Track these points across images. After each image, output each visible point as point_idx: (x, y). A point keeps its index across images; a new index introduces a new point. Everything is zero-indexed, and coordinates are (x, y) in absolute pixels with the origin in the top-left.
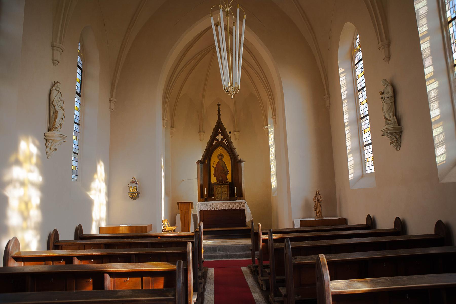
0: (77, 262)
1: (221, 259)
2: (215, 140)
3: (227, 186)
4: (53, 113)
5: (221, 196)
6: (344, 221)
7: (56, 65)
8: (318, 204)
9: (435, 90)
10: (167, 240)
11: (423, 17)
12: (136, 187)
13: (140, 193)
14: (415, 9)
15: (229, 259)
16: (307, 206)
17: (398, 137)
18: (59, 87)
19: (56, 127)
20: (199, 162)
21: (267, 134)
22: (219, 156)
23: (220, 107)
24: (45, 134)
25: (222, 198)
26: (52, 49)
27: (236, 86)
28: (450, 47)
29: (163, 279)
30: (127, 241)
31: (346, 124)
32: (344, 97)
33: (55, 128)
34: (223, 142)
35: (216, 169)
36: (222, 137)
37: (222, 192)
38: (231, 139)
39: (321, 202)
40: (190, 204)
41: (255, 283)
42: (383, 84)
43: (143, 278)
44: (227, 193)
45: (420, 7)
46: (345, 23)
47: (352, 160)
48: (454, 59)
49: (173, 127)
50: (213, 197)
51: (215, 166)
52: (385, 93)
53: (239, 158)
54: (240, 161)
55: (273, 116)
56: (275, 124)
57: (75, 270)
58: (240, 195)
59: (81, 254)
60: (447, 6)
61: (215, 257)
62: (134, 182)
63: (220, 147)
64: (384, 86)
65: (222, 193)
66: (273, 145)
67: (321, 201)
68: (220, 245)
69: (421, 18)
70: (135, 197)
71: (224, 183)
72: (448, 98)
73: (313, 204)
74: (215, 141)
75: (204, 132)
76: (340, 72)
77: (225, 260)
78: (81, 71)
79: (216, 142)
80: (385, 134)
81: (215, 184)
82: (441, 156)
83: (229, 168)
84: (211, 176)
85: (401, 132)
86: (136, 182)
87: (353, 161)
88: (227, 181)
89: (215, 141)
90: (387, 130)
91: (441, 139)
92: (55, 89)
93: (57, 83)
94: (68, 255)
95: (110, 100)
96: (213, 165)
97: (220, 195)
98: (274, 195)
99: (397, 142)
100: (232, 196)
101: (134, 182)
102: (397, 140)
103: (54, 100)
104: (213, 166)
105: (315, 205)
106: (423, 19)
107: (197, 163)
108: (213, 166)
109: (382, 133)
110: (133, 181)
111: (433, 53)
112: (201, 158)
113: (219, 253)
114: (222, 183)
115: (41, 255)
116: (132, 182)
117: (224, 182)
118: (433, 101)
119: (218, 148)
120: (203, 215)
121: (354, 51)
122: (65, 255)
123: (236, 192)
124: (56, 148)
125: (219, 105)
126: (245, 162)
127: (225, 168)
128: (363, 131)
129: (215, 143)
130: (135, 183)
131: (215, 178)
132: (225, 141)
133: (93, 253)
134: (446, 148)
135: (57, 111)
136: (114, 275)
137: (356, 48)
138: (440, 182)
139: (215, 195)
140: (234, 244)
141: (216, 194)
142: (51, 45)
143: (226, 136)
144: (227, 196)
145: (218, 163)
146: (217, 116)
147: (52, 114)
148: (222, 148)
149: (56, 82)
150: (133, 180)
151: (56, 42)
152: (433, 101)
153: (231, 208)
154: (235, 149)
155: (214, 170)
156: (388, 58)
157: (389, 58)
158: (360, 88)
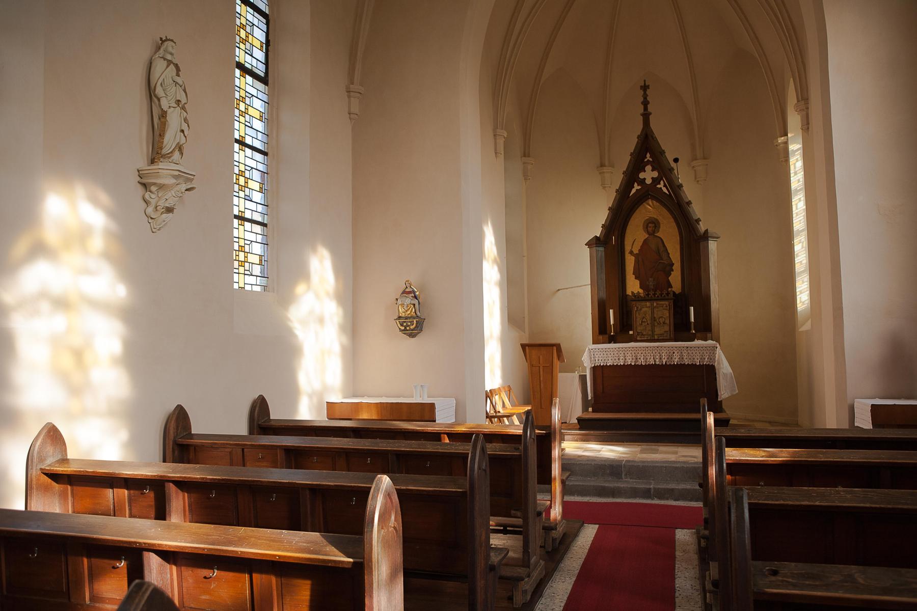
1: (629, 498)
2: (658, 186)
3: (667, 303)
4: (158, 117)
5: (650, 328)
10: (437, 449)
12: (414, 305)
13: (425, 319)
15: (653, 499)
18: (170, 49)
19: (168, 154)
20: (594, 243)
23: (647, 92)
24: (140, 172)
25: (653, 335)
33: (164, 156)
34: (658, 186)
36: (655, 174)
37: (653, 319)
38: (679, 178)
40: (555, 348)
41: (697, 590)
44: (667, 321)
49: (529, 156)
50: (631, 332)
51: (636, 251)
53: (702, 227)
54: (706, 236)
55: (798, 101)
56: (806, 126)
58: (705, 328)
59: (180, 477)
61: (613, 493)
62: (410, 293)
63: (650, 200)
65: (655, 320)
66: (800, 190)
68: (635, 462)
70: (412, 330)
71: (658, 296)
74: (636, 184)
77: (643, 504)
78: (264, 21)
79: (639, 187)
81: (637, 298)
83: (675, 254)
86: (414, 292)
88: (670, 289)
89: (636, 184)
92: (161, 56)
93: (167, 40)
94: (151, 475)
96: (632, 248)
97: (649, 328)
101: (410, 293)
104: (631, 253)
107: (589, 244)
110: (407, 290)
112: (598, 232)
113: (625, 483)
116: (404, 292)
117: (658, 293)
120: (603, 377)
123: (692, 320)
124: (168, 205)
125: (645, 88)
129: (637, 190)
131: (637, 282)
139: (636, 327)
140: (672, 458)
141: (638, 324)
143: (665, 171)
144: (667, 328)
145: (645, 242)
148: (655, 202)
149: (164, 38)
150: (407, 287)
153: (676, 360)
154: (689, 203)
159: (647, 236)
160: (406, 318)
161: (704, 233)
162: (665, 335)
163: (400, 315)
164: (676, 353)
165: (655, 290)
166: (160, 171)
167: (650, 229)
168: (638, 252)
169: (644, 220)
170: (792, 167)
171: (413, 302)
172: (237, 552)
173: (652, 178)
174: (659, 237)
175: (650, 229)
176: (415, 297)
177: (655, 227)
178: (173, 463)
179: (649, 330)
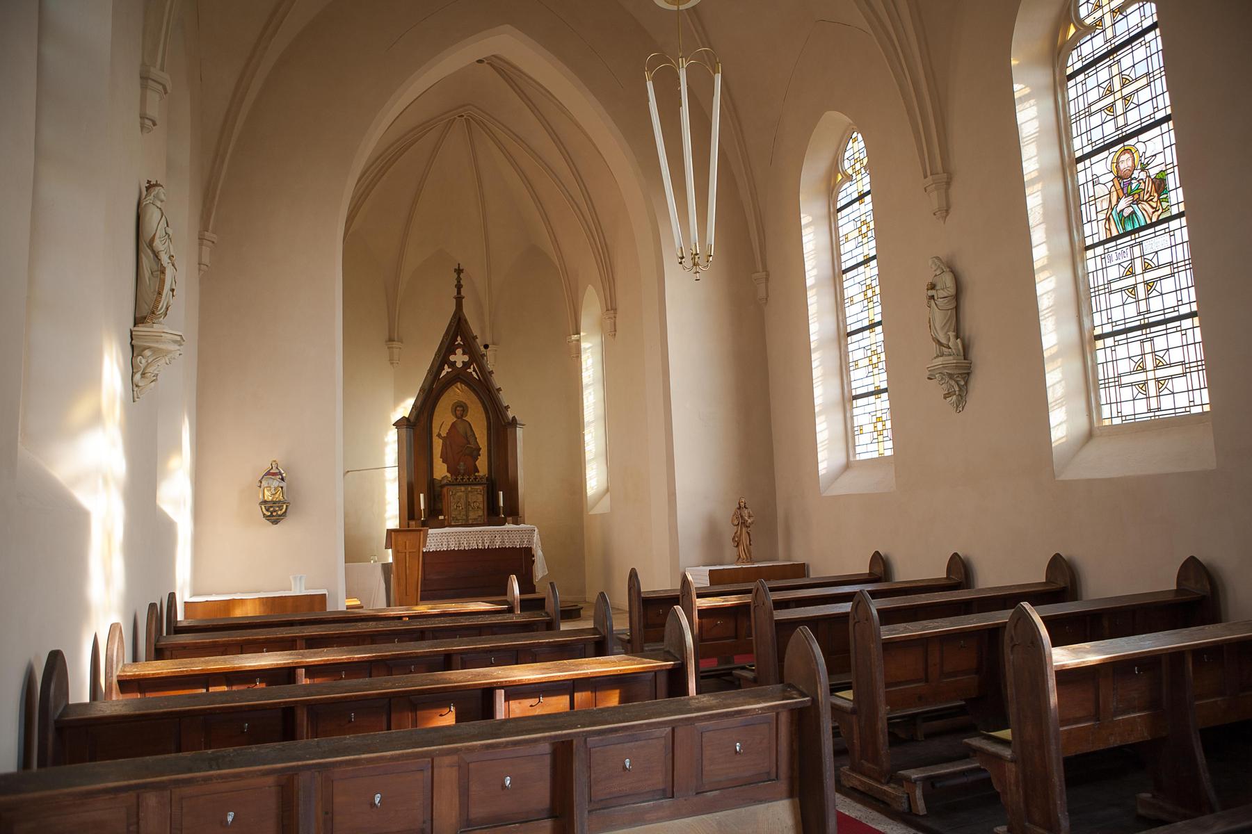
0: (304, 680)
3: (481, 487)
5: (465, 513)
6: (800, 570)
8: (744, 529)
11: (1030, 141)
14: (1017, 122)
16: (712, 537)
17: (962, 383)
18: (163, 197)
21: (575, 355)
22: (456, 408)
24: (134, 333)
25: (467, 520)
26: (141, 84)
28: (1079, 211)
30: (365, 627)
31: (813, 346)
32: (810, 281)
34: (468, 370)
35: (448, 443)
36: (466, 358)
37: (468, 504)
42: (934, 268)
44: (481, 506)
46: (826, 113)
47: (824, 430)
50: (441, 517)
51: (444, 434)
53: (510, 414)
54: (514, 423)
56: (610, 331)
58: (513, 512)
62: (274, 474)
63: (459, 383)
64: (935, 271)
69: (1026, 143)
70: (280, 516)
72: (1071, 312)
73: (729, 530)
74: (446, 367)
76: (803, 222)
79: (450, 370)
80: (937, 376)
83: (482, 441)
85: (968, 374)
87: (827, 431)
88: (476, 474)
89: (446, 367)
91: (1059, 394)
93: (157, 185)
94: (285, 664)
95: (201, 239)
98: (597, 510)
99: (960, 395)
100: (493, 515)
101: (274, 474)
102: (960, 390)
103: (155, 235)
104: (439, 435)
105: (737, 532)
108: (439, 435)
109: (930, 373)
115: (208, 670)
116: (268, 473)
117: (466, 477)
118: (1047, 316)
119: (453, 387)
121: (836, 178)
123: (501, 504)
126: (523, 425)
127: (472, 440)
131: (445, 466)
132: (474, 367)
133: (356, 656)
135: (165, 268)
136: (516, 691)
137: (842, 170)
138: (1057, 479)
143: (475, 357)
144: (480, 513)
145: (453, 425)
146: (455, 300)
147: (146, 273)
148: (463, 386)
152: (1047, 316)
155: (441, 445)
156: (946, 211)
157: (947, 211)
158: (849, 264)
159: (455, 419)
163: (266, 498)
166: (163, 334)
167: (458, 413)
168: (445, 435)
170: (584, 363)
171: (281, 485)
172: (587, 673)
173: (463, 362)
175: (458, 413)
176: (282, 479)
177: (464, 411)
178: (306, 649)
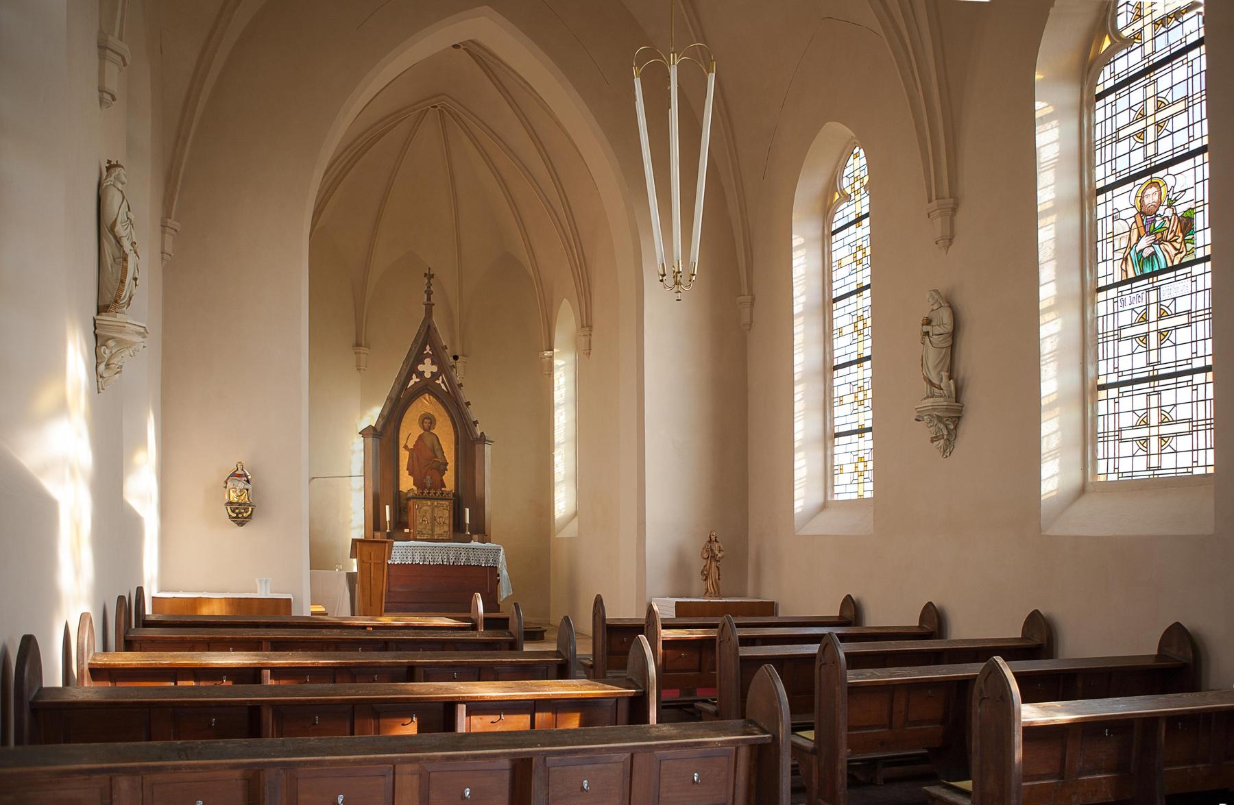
2: (437, 381)
3: (447, 503)
5: (430, 528)
6: (769, 608)
7: (107, 106)
9: (1054, 337)
16: (680, 568)
18: (123, 179)
21: (547, 373)
25: (433, 535)
26: (99, 54)
27: (679, 269)
29: (578, 718)
31: (796, 378)
32: (797, 309)
35: (415, 455)
36: (435, 369)
37: (434, 519)
39: (719, 561)
43: (536, 714)
44: (447, 522)
45: (1045, 144)
47: (803, 467)
48: (1099, 276)
50: (407, 530)
51: (411, 446)
52: (933, 323)
54: (483, 439)
57: (412, 694)
58: (480, 530)
60: (1098, 152)
62: (240, 476)
65: (435, 520)
67: (720, 558)
70: (245, 518)
72: (1075, 358)
73: (698, 564)
74: (414, 376)
75: (368, 346)
76: (795, 243)
79: (418, 380)
82: (1048, 480)
83: (450, 456)
84: (401, 472)
85: (959, 418)
86: (246, 476)
88: (443, 489)
89: (414, 376)
90: (946, 408)
91: (1054, 445)
93: (117, 165)
95: (164, 226)
96: (407, 442)
97: (429, 527)
100: (458, 530)
101: (240, 476)
102: (949, 434)
103: (116, 219)
104: (406, 447)
106: (1048, 172)
108: (406, 447)
111: (1058, 253)
114: (435, 494)
116: (234, 475)
117: (432, 492)
118: (1048, 361)
121: (833, 196)
122: (244, 664)
128: (1099, 435)
130: (244, 479)
131: (411, 479)
132: (443, 378)
134: (1060, 464)
136: (478, 707)
138: (1043, 533)
141: (418, 522)
142: (98, 43)
144: (446, 529)
147: (109, 260)
148: (431, 397)
150: (237, 469)
151: (113, 35)
152: (1048, 361)
156: (949, 240)
157: (951, 240)
159: (423, 432)
160: (240, 504)
161: (481, 436)
162: (445, 535)
163: (231, 499)
164: (463, 553)
165: (430, 489)
166: (126, 325)
169: (419, 415)
170: (556, 382)
174: (435, 435)
176: (248, 481)
179: (429, 530)
